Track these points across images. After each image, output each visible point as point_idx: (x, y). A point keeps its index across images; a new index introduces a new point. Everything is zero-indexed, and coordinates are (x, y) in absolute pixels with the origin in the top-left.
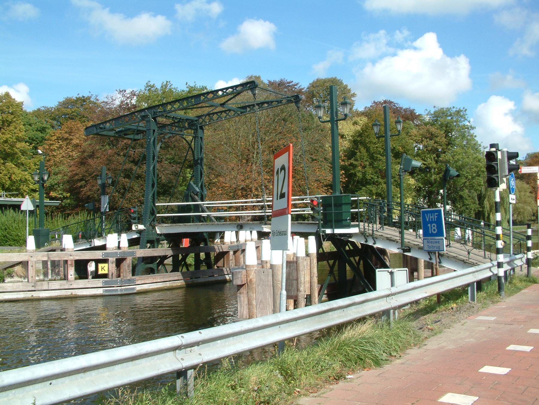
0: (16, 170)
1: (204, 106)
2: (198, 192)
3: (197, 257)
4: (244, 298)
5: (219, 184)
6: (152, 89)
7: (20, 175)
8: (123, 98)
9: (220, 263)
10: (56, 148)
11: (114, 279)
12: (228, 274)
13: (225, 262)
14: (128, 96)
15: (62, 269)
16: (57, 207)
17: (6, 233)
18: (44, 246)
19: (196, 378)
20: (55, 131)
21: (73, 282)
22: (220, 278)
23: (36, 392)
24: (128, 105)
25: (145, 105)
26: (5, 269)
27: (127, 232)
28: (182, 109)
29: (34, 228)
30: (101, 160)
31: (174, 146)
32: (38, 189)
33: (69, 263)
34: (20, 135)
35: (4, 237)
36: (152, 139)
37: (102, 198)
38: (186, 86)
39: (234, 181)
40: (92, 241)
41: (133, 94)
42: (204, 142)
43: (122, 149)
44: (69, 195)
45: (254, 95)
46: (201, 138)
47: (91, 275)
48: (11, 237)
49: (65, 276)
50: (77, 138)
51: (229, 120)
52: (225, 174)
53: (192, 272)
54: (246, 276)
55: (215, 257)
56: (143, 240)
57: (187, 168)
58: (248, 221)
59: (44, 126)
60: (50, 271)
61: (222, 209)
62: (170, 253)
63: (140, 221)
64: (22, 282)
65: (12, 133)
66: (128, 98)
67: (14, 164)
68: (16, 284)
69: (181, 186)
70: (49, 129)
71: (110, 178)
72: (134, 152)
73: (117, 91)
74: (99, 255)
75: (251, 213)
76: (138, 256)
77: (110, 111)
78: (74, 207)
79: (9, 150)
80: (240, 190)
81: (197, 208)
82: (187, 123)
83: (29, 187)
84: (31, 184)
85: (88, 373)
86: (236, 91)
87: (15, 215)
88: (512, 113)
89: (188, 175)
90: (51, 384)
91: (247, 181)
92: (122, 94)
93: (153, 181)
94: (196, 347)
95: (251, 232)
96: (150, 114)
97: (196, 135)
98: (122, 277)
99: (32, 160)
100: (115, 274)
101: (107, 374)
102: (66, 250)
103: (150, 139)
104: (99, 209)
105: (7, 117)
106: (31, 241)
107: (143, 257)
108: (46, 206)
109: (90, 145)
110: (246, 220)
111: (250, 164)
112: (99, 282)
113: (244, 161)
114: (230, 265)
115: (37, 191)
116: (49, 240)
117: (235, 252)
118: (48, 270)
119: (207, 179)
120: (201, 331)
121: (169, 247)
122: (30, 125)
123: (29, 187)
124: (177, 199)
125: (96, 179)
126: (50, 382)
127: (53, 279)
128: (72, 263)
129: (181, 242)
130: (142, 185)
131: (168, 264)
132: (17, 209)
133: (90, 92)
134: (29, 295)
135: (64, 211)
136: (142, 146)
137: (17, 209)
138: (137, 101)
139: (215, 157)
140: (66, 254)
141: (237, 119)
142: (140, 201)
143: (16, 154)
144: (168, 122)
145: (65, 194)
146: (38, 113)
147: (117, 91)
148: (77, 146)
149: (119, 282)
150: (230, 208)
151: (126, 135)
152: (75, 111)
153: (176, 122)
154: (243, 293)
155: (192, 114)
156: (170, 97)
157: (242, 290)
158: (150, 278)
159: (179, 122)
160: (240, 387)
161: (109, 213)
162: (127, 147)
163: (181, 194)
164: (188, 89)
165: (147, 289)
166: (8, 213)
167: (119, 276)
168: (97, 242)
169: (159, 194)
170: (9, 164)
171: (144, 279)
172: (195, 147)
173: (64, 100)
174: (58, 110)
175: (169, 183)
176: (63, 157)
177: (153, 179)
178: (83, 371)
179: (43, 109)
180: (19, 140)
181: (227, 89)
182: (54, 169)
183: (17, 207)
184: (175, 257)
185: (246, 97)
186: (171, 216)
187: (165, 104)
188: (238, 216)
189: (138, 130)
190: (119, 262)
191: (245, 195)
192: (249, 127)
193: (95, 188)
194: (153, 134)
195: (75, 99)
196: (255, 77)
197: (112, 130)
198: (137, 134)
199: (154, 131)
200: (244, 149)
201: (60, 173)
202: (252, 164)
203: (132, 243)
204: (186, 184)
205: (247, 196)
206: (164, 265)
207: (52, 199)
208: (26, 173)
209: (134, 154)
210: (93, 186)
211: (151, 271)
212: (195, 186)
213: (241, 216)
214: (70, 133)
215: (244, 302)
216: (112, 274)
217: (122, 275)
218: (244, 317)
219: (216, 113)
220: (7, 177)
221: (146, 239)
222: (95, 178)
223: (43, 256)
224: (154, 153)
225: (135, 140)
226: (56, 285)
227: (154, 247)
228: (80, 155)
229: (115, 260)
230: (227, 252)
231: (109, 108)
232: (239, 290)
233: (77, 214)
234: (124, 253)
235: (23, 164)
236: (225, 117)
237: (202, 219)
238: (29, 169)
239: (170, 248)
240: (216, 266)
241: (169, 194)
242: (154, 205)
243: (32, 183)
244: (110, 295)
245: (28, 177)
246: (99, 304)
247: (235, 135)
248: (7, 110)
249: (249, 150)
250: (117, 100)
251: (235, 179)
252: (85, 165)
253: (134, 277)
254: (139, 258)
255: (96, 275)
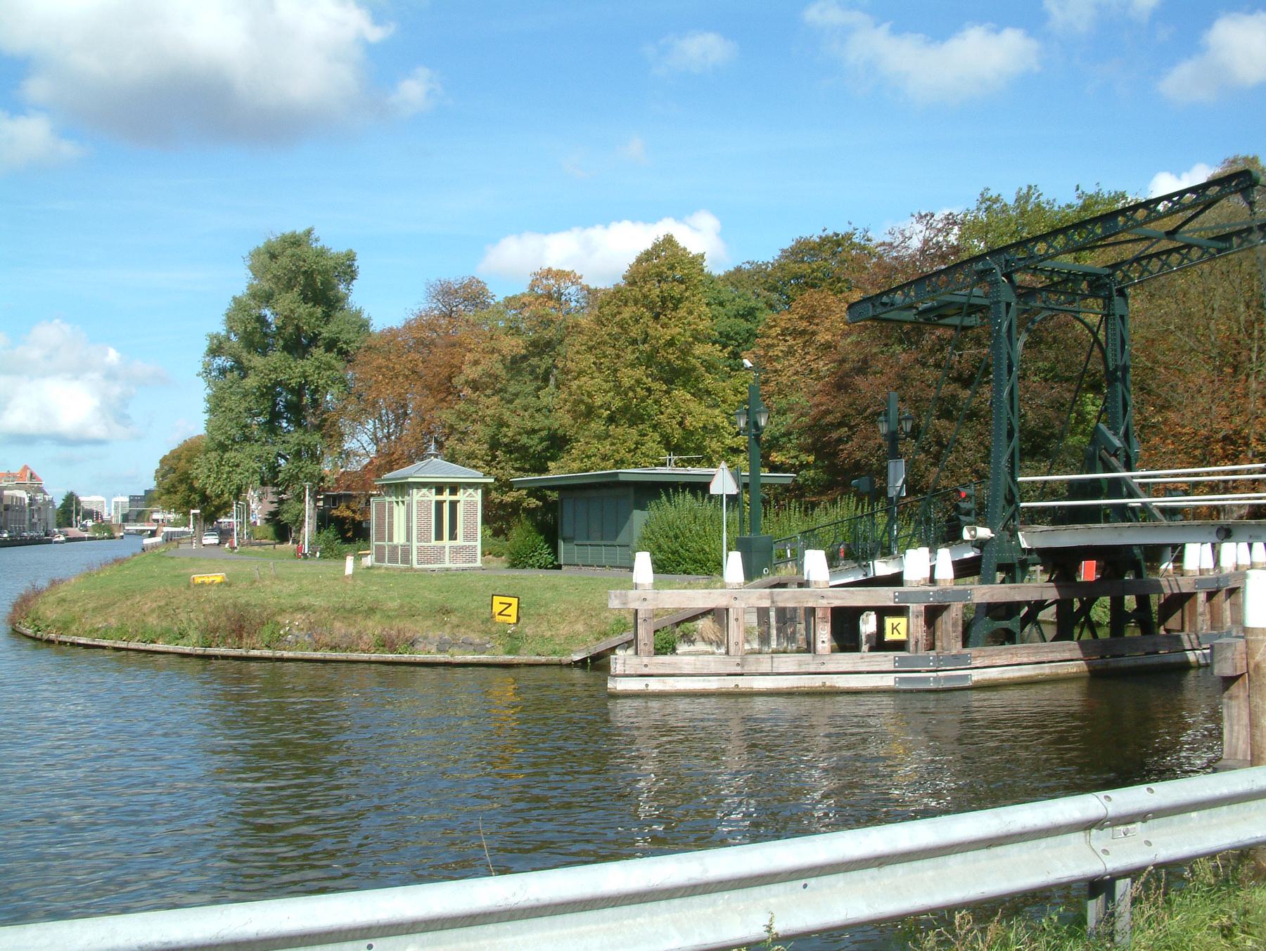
0: (694, 406)
1: (1122, 239)
2: (1118, 449)
3: (1117, 605)
4: (1239, 708)
5: (1165, 429)
6: (995, 206)
7: (704, 418)
8: (928, 232)
9: (1173, 623)
10: (780, 354)
11: (920, 654)
12: (1193, 650)
13: (1187, 619)
14: (940, 225)
15: (801, 627)
16: (786, 488)
17: (677, 544)
18: (760, 575)
19: (1135, 901)
20: (776, 316)
21: (828, 658)
22: (1174, 658)
23: (772, 900)
24: (941, 247)
25: (980, 246)
26: (678, 624)
27: (951, 545)
28: (1069, 252)
29: (738, 535)
30: (884, 378)
31: (1055, 339)
32: (742, 448)
33: (819, 614)
34: (701, 327)
35: (673, 553)
36: (1005, 325)
37: (891, 464)
38: (1075, 195)
39: (1203, 420)
40: (869, 566)
41: (950, 221)
42: (1130, 324)
43: (932, 352)
44: (811, 458)
45: (1251, 204)
46: (1122, 317)
47: (867, 642)
48: (687, 554)
49: (808, 643)
50: (827, 330)
51: (1183, 270)
52: (1180, 403)
53: (1104, 641)
54: (1244, 656)
55: (1160, 606)
56: (989, 563)
57: (1086, 391)
58: (1241, 517)
59: (752, 304)
60: (774, 632)
61: (1175, 489)
62: (1051, 594)
63: (981, 516)
64: (713, 653)
65: (683, 323)
66: (939, 230)
67: (690, 393)
68: (701, 658)
69: (1073, 433)
70: (762, 310)
71: (906, 419)
72: (960, 356)
73: (913, 216)
74: (885, 596)
75: (1249, 499)
76: (977, 600)
77: (901, 263)
78: (824, 488)
79: (678, 362)
80: (1217, 441)
81: (1115, 488)
82: (1085, 282)
83: (723, 443)
84: (727, 436)
85: (887, 869)
86: (1204, 196)
87: (696, 505)
88: (216, 336)
89: (1090, 408)
90: (805, 886)
91: (1238, 420)
92: (925, 222)
93: (1010, 424)
94: (1138, 826)
95: (1250, 546)
96: (996, 267)
97: (1109, 310)
98: (938, 649)
99: (728, 382)
100: (923, 642)
101: (930, 873)
102: (812, 584)
103: (1000, 325)
104: (883, 492)
105: (672, 289)
106: (734, 564)
107: (989, 604)
108: (763, 485)
109: (858, 343)
110: (1235, 515)
111: (1243, 377)
112: (886, 660)
113: (1228, 370)
114: (1199, 626)
115: (742, 452)
116: (772, 562)
117: (1210, 596)
118: (769, 628)
119: (1138, 417)
120: (1152, 786)
121: (1049, 581)
122: (721, 304)
123: (723, 443)
124: (1065, 467)
125: (873, 422)
126: (803, 882)
127: (781, 649)
128: (825, 614)
129: (1077, 569)
130: (981, 434)
131: (1045, 622)
132: (700, 493)
133: (850, 223)
134: (729, 684)
135: (803, 495)
136: (978, 342)
137: (700, 493)
138: (960, 237)
139: (1155, 362)
140: (811, 595)
141: (1206, 267)
142: (976, 472)
143: (694, 369)
144: (1039, 281)
145: (804, 458)
146: (736, 277)
147: (913, 216)
148: (827, 346)
149: (931, 661)
150: (1194, 488)
151: (941, 317)
152: (819, 268)
153: (1058, 283)
154: (1237, 697)
155: (1094, 261)
156: (1038, 222)
157: (1234, 689)
158: (1004, 654)
159: (1065, 281)
160: (1243, 932)
161: (905, 501)
162: (941, 345)
163: (1073, 455)
164: (1080, 202)
165: (996, 680)
166: (680, 502)
167: (932, 647)
168: (882, 568)
169: (1024, 454)
170: (680, 393)
171: (992, 656)
172: (1107, 339)
173: (794, 243)
174: (781, 267)
175: (1045, 427)
176: (796, 373)
177: (1009, 419)
178: (877, 863)
179: (748, 266)
180: (697, 337)
181: (1181, 194)
182: (779, 402)
183: (699, 488)
184: (1063, 605)
185: (1232, 208)
186: (1054, 507)
187: (1029, 240)
188: (1215, 507)
189: (971, 306)
190: (933, 614)
191: (1233, 454)
192: (1236, 284)
193: (871, 443)
194: (1007, 312)
195: (818, 240)
196: (1245, 159)
197: (910, 307)
198: (969, 315)
199: (1008, 305)
200: (1226, 340)
201: (791, 409)
202: (1248, 376)
203: (963, 569)
204: (1084, 430)
205: (1237, 457)
206: (1037, 623)
207: (774, 468)
208: (717, 412)
209: (959, 362)
210: (867, 438)
211: (1007, 637)
212: (1109, 434)
213: (1223, 506)
214: (810, 319)
215: (1238, 720)
216: (917, 642)
217: (938, 644)
218: (1240, 757)
219: (1157, 255)
220: (674, 422)
221: (994, 561)
222: (873, 419)
223: (761, 598)
224: (1009, 358)
225: (965, 328)
226: (789, 662)
227: (1013, 581)
228: (834, 367)
229: (923, 608)
230: (1190, 596)
231: (896, 258)
232: (1226, 688)
233: (834, 502)
234: (944, 592)
235: (708, 393)
236: (1180, 264)
237: (1129, 514)
238: (724, 402)
239: (1052, 584)
240: (1162, 628)
241: (1047, 455)
242: (1014, 480)
243: (729, 434)
244: (911, 691)
245: (721, 420)
246: (883, 713)
247: (1201, 306)
248: (669, 272)
249: (1237, 343)
250: (914, 236)
251: (1207, 413)
252: (846, 392)
253: (966, 651)
254: (978, 605)
255: (880, 643)
